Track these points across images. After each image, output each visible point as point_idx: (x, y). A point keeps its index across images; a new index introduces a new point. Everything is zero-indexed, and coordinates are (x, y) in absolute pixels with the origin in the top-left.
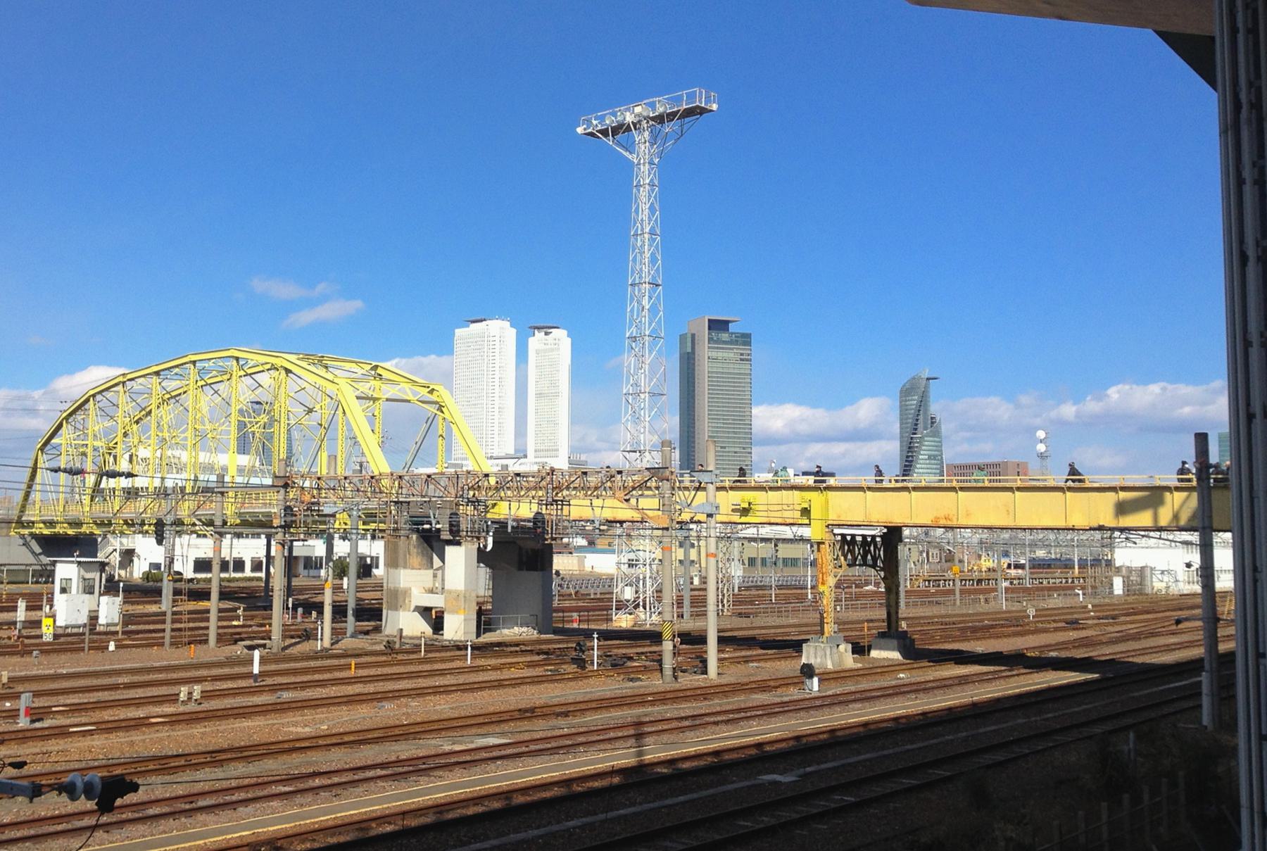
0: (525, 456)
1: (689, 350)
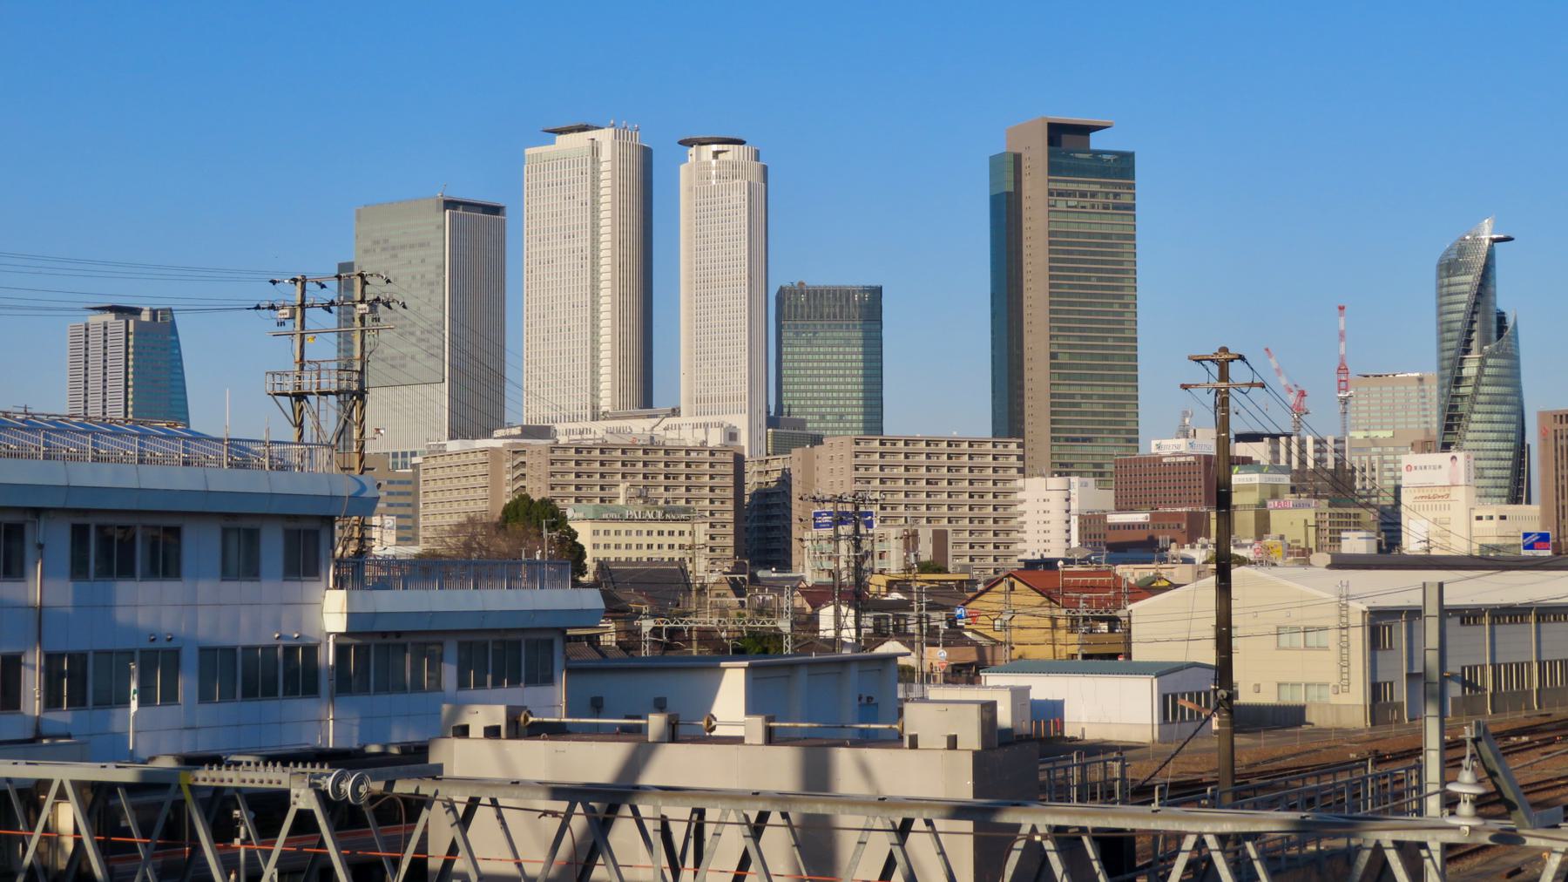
0: (675, 412)
1: (1010, 188)
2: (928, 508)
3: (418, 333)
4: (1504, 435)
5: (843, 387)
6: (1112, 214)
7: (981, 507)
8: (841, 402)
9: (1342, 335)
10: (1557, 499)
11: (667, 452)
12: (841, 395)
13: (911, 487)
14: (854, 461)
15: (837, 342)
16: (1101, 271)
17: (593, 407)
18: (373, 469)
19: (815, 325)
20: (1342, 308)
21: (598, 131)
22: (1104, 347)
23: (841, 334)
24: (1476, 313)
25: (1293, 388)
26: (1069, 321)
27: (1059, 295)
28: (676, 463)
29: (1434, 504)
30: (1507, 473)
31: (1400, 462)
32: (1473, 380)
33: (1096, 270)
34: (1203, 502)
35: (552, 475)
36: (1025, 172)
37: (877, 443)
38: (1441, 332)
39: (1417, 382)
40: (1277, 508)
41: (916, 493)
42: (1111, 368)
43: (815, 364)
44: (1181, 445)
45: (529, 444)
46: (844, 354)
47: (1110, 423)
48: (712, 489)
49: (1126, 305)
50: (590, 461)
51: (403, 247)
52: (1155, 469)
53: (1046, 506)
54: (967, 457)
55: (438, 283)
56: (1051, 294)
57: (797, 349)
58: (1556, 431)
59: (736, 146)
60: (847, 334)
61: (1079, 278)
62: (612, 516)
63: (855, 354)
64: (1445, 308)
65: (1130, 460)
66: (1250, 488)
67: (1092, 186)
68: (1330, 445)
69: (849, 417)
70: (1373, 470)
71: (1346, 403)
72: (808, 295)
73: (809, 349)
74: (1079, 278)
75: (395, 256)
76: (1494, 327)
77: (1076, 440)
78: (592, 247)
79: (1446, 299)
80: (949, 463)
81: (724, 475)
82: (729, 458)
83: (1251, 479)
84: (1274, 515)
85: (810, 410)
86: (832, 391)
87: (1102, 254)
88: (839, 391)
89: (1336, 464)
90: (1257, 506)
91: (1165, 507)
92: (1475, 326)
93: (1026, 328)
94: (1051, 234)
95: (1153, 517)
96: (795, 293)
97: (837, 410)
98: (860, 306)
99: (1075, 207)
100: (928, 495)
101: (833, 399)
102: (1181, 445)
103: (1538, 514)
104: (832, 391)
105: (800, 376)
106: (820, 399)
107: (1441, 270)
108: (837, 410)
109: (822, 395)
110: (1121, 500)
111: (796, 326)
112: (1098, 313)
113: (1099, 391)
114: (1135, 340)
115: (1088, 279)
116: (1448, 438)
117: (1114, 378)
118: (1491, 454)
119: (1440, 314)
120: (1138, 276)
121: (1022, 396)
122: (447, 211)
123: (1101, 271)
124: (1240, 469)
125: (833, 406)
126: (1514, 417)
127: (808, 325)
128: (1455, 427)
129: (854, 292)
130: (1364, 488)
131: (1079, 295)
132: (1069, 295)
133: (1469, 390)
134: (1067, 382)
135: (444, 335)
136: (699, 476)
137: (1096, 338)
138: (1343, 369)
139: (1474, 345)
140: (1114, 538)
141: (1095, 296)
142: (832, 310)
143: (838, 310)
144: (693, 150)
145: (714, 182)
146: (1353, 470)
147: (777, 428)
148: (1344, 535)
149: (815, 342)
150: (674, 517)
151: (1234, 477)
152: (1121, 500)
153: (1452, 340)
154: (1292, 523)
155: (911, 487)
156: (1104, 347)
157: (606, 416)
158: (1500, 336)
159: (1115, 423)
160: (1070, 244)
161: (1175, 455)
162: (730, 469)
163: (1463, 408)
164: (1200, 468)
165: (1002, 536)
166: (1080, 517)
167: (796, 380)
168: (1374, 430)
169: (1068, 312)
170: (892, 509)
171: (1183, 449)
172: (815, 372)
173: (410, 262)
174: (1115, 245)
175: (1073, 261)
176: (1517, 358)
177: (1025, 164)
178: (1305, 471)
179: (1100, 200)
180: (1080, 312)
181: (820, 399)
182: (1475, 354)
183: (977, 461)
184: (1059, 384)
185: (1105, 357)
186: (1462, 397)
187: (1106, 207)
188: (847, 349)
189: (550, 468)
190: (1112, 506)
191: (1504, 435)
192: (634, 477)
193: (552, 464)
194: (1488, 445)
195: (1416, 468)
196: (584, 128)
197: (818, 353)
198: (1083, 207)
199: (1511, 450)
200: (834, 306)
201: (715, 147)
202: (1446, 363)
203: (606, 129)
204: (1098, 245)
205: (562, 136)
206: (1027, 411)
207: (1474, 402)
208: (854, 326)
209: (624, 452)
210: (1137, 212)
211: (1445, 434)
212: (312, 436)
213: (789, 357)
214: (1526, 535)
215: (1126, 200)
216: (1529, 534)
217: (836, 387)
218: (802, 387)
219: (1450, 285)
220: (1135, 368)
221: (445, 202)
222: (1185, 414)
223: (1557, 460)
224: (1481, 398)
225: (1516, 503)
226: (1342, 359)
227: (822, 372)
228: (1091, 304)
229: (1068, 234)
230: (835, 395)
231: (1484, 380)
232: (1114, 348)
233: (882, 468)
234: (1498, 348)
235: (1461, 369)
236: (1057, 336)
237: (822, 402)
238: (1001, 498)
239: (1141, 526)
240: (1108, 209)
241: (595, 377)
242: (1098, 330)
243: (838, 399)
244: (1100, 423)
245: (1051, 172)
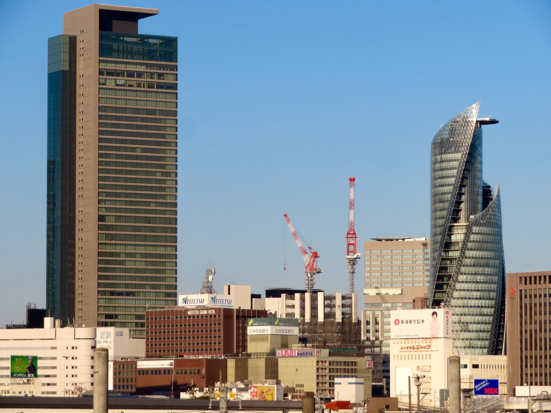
4: (486, 294)
6: (156, 92)
9: (352, 204)
10: (521, 351)
16: (146, 142)
20: (352, 180)
22: (147, 211)
24: (465, 186)
25: (308, 250)
26: (116, 187)
27: (107, 163)
29: (417, 353)
30: (489, 327)
31: (389, 316)
32: (460, 245)
33: (141, 143)
34: (222, 350)
36: (79, 52)
38: (434, 203)
39: (422, 247)
40: (283, 357)
42: (153, 229)
44: (206, 299)
47: (152, 279)
49: (168, 174)
52: (181, 321)
53: (74, 353)
56: (100, 163)
58: (521, 291)
61: (126, 149)
64: (438, 181)
65: (160, 312)
66: (262, 338)
67: (138, 67)
68: (338, 302)
70: (377, 323)
71: (354, 264)
74: (126, 149)
76: (480, 199)
77: (120, 294)
79: (438, 174)
83: (264, 331)
84: (282, 363)
87: (147, 127)
89: (343, 319)
90: (268, 354)
91: (189, 354)
92: (463, 198)
93: (78, 193)
94: (101, 109)
95: (177, 363)
99: (123, 85)
102: (206, 299)
103: (505, 364)
107: (435, 148)
110: (152, 348)
112: (142, 180)
113: (142, 250)
114: (175, 205)
115: (134, 150)
116: (439, 296)
117: (155, 238)
118: (475, 310)
119: (434, 186)
120: (179, 148)
121: (74, 254)
123: (146, 142)
124: (254, 322)
126: (495, 278)
128: (445, 287)
130: (368, 339)
131: (125, 164)
132: (117, 164)
133: (457, 254)
134: (113, 242)
137: (139, 203)
138: (352, 234)
139: (462, 214)
140: (143, 382)
141: (141, 165)
146: (359, 323)
148: (336, 380)
151: (249, 328)
152: (152, 348)
153: (443, 210)
154: (297, 370)
156: (147, 211)
158: (484, 207)
159: (156, 279)
160: (118, 118)
161: (199, 308)
163: (452, 270)
164: (219, 320)
166: (115, 363)
168: (385, 287)
169: (115, 179)
171: (206, 303)
174: (159, 121)
175: (120, 134)
176: (499, 227)
177: (79, 46)
178: (316, 324)
179: (146, 79)
180: (126, 180)
182: (462, 222)
184: (106, 244)
185: (148, 220)
186: (451, 260)
187: (151, 86)
190: (143, 354)
191: (486, 294)
194: (472, 302)
195: (402, 322)
198: (130, 86)
199: (492, 307)
202: (438, 230)
204: (143, 120)
206: (78, 268)
207: (461, 264)
210: (179, 91)
211: (435, 292)
212: (45, 368)
214: (477, 382)
215: (169, 80)
216: (481, 381)
219: (442, 161)
220: (175, 230)
222: (209, 272)
223: (521, 316)
224: (467, 261)
225: (496, 354)
226: (352, 224)
228: (136, 172)
229: (116, 109)
231: (470, 245)
232: (156, 212)
234: (483, 217)
235: (450, 235)
236: (105, 201)
239: (167, 371)
240: (153, 87)
242: (142, 196)
244: (142, 278)
245: (101, 54)
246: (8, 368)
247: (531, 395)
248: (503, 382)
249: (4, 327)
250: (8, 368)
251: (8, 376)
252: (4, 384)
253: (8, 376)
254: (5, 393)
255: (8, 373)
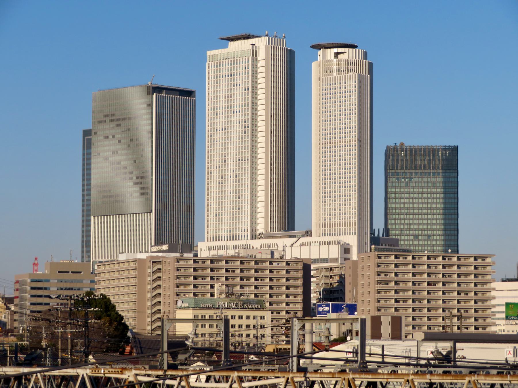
0: (308, 234)
2: (429, 301)
3: (134, 178)
5: (430, 216)
7: (466, 301)
8: (429, 227)
11: (256, 263)
12: (429, 222)
13: (417, 287)
14: (377, 269)
15: (426, 185)
17: (252, 230)
18: (80, 272)
19: (411, 173)
21: (257, 39)
23: (429, 180)
28: (263, 270)
35: (178, 277)
37: (393, 257)
41: (420, 291)
43: (411, 201)
45: (164, 257)
46: (431, 193)
48: (288, 288)
50: (203, 269)
51: (125, 119)
54: (456, 267)
55: (148, 144)
57: (398, 190)
59: (351, 49)
60: (433, 180)
62: (207, 305)
63: (438, 193)
69: (435, 238)
72: (406, 151)
73: (406, 190)
75: (118, 125)
78: (252, 119)
80: (444, 271)
81: (295, 279)
82: (300, 266)
85: (408, 232)
86: (423, 219)
88: (427, 219)
96: (397, 151)
97: (426, 232)
98: (443, 160)
100: (429, 293)
101: (423, 224)
104: (423, 219)
105: (401, 209)
106: (414, 224)
108: (426, 232)
109: (416, 222)
111: (398, 174)
122: (155, 94)
125: (423, 230)
127: (406, 173)
129: (438, 150)
135: (152, 179)
136: (278, 279)
142: (423, 162)
143: (427, 163)
144: (320, 52)
145: (335, 74)
147: (379, 245)
149: (411, 185)
150: (250, 307)
155: (417, 287)
157: (261, 236)
162: (300, 274)
165: (480, 321)
167: (397, 211)
170: (404, 302)
172: (411, 206)
173: (129, 129)
181: (414, 224)
183: (463, 270)
188: (434, 190)
189: (177, 273)
192: (234, 279)
193: (178, 270)
196: (247, 37)
197: (414, 193)
200: (424, 160)
201: (336, 50)
203: (263, 38)
205: (232, 42)
208: (439, 174)
209: (227, 262)
213: (393, 195)
217: (426, 216)
218: (402, 216)
221: (153, 88)
227: (415, 206)
230: (425, 222)
233: (396, 274)
237: (416, 227)
238: (480, 295)
241: (254, 209)
243: (427, 224)
246: (503, 312)
247: (266, 312)
248: (416, 348)
249: (500, 280)
250: (503, 312)
251: (503, 319)
252: (501, 325)
253: (503, 319)
254: (501, 331)
255: (504, 315)
